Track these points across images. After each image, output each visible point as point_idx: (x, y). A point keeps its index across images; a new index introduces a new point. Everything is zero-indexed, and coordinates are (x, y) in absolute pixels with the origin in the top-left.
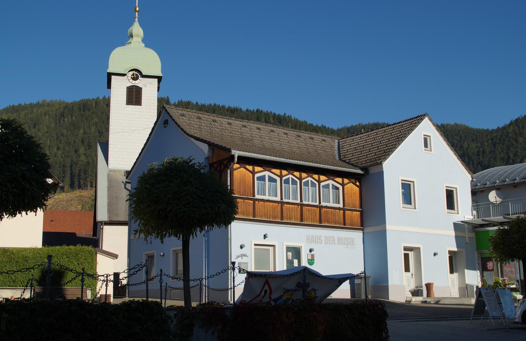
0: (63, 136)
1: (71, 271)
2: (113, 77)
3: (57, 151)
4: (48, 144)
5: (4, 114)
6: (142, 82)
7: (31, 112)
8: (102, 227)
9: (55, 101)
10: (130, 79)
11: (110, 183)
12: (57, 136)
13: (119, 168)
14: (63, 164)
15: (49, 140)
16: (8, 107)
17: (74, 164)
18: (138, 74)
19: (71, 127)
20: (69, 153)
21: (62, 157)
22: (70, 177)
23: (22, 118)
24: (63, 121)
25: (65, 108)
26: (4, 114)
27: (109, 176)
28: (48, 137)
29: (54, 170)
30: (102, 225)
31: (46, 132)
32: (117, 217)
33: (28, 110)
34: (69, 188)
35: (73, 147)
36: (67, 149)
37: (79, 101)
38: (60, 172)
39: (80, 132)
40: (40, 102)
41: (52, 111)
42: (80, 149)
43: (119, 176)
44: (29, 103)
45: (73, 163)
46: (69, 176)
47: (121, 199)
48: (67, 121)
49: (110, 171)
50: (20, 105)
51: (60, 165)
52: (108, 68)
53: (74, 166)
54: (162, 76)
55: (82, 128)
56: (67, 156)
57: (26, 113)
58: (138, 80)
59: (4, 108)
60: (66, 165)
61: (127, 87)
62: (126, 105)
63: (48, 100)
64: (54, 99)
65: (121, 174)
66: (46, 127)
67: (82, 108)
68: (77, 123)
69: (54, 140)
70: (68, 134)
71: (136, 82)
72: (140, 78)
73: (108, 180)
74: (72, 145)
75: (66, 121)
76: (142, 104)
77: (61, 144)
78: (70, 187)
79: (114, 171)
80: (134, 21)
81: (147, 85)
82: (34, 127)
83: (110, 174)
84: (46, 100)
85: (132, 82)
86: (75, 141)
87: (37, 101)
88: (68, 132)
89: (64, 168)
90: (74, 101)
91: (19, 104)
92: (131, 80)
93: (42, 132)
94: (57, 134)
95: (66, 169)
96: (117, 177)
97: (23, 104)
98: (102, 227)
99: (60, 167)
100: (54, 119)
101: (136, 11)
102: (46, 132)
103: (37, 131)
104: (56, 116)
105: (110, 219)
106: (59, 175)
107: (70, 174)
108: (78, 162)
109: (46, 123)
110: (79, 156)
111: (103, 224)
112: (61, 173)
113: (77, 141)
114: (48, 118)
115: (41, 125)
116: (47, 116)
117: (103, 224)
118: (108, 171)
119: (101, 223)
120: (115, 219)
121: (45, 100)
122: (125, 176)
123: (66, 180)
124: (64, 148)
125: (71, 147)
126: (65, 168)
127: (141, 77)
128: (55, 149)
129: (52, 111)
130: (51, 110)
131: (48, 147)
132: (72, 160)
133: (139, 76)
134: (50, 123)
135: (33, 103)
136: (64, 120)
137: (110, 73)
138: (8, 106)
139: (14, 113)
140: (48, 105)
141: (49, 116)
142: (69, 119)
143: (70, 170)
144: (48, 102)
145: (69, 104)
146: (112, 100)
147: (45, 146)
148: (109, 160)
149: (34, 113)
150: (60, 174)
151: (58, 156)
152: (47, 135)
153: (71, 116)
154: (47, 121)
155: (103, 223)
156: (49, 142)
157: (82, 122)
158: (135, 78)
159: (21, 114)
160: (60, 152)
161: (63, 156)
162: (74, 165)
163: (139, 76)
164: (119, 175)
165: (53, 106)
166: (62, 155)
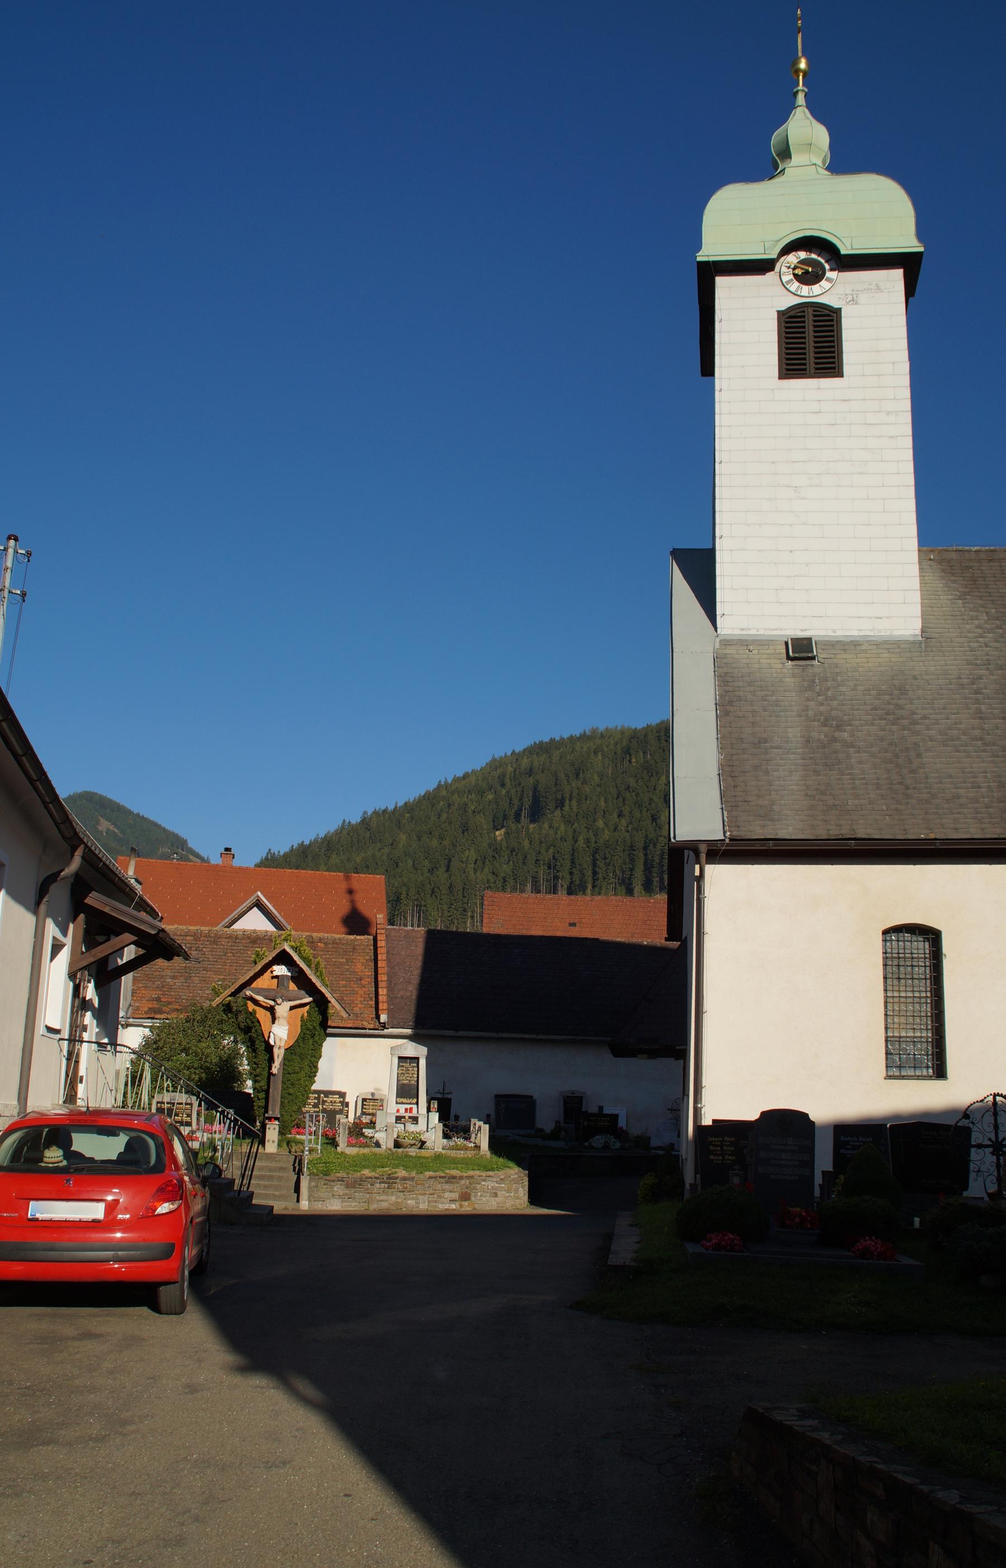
0: (628, 790)
1: (330, 1144)
2: (723, 284)
3: (618, 820)
4: (602, 808)
5: (525, 757)
6: (839, 289)
7: (571, 750)
8: (697, 873)
9: (613, 728)
10: (788, 282)
11: (727, 688)
12: (618, 790)
13: (761, 632)
14: (629, 844)
15: (603, 799)
16: (532, 745)
17: (650, 843)
18: (823, 261)
19: (643, 773)
20: (642, 822)
21: (628, 831)
22: (643, 869)
23: (556, 763)
24: (628, 763)
25: (632, 738)
26: (525, 757)
27: (718, 660)
28: (601, 794)
29: (615, 856)
30: (698, 862)
31: (598, 785)
32: (769, 823)
33: (566, 747)
34: (643, 892)
35: (647, 811)
36: (637, 815)
37: (657, 725)
38: (624, 860)
39: (660, 782)
40: (588, 733)
41: (607, 746)
42: (661, 815)
43: (762, 661)
44: (568, 736)
45: (648, 841)
46: (642, 867)
47: (778, 747)
48: (637, 762)
49: (726, 643)
50: (552, 740)
51: (625, 847)
52: (699, 247)
53: (651, 847)
54: (922, 249)
55: (663, 773)
56: (638, 829)
57: (562, 753)
58: (823, 283)
59: (526, 747)
60: (635, 846)
61: (778, 312)
62: (780, 378)
63: (602, 728)
64: (611, 726)
65: (770, 651)
66: (598, 776)
67: (664, 737)
68: (654, 764)
69: (613, 798)
70: (638, 786)
71: (816, 289)
72: (829, 274)
73: (720, 676)
74: (645, 807)
75: (634, 762)
76: (846, 369)
77: (626, 806)
78: (645, 890)
79: (744, 643)
80: (792, 106)
81: (863, 298)
82: (577, 776)
83: (725, 656)
84: (597, 728)
85: (797, 290)
86: (652, 799)
87: (582, 731)
88: (637, 782)
89: (632, 852)
90: (647, 724)
91: (551, 739)
92: (795, 286)
93: (591, 785)
94: (617, 788)
95: (636, 854)
96: (757, 666)
97: (557, 738)
98: (697, 873)
99: (624, 851)
100: (612, 759)
101: (797, 71)
102: (598, 785)
103: (582, 784)
104: (615, 753)
105: (735, 833)
106: (624, 866)
107: (642, 863)
108: (657, 840)
109: (597, 769)
110: (660, 828)
111: (703, 857)
112: (628, 863)
113: (655, 798)
114: (601, 758)
115: (589, 772)
116: (600, 754)
117: (703, 857)
118: (717, 646)
119: (693, 846)
120: (757, 830)
121: (595, 727)
122: (789, 658)
123: (636, 874)
124: (630, 813)
125: (644, 810)
126: (634, 852)
127: (832, 270)
128: (615, 815)
129: (607, 746)
130: (606, 743)
131: (602, 813)
132: (646, 836)
133: (827, 266)
134: (604, 768)
135: (575, 735)
136: (630, 762)
137: (708, 263)
138: (533, 744)
139: (542, 755)
140: (602, 736)
141: (602, 754)
142: (640, 757)
143: (643, 855)
144: (601, 732)
145: (639, 731)
146: (720, 451)
147: (596, 811)
148: (718, 599)
149: (575, 753)
150: (625, 864)
151: (619, 829)
152: (599, 789)
153: (644, 753)
154: (600, 764)
155: (703, 849)
156: (603, 804)
157: (664, 762)
158: (810, 276)
159: (554, 755)
160: (624, 822)
161: (629, 829)
162: (651, 845)
163: (827, 266)
164: (765, 656)
165: (609, 737)
166: (628, 826)
